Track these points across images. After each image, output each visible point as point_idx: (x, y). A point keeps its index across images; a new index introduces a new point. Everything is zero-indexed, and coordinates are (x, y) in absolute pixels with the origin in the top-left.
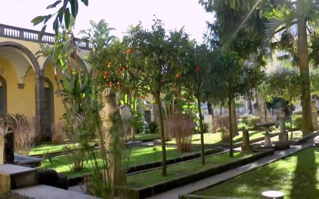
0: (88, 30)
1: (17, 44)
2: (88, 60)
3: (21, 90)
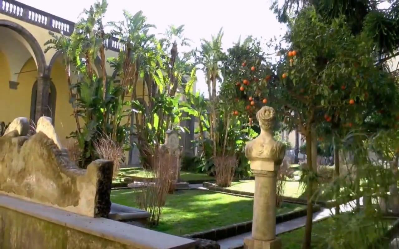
0: (119, 22)
1: (18, 25)
2: (114, 62)
3: (12, 91)
